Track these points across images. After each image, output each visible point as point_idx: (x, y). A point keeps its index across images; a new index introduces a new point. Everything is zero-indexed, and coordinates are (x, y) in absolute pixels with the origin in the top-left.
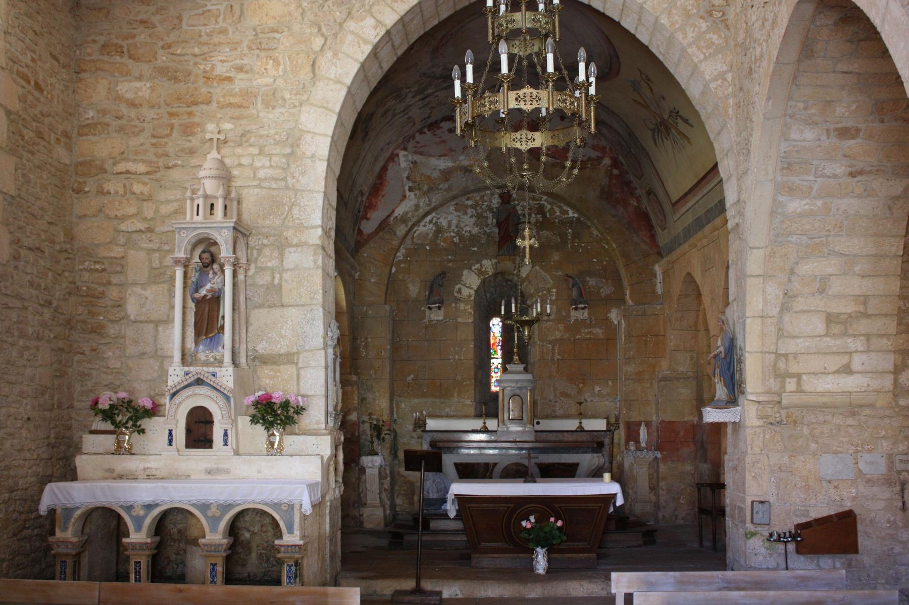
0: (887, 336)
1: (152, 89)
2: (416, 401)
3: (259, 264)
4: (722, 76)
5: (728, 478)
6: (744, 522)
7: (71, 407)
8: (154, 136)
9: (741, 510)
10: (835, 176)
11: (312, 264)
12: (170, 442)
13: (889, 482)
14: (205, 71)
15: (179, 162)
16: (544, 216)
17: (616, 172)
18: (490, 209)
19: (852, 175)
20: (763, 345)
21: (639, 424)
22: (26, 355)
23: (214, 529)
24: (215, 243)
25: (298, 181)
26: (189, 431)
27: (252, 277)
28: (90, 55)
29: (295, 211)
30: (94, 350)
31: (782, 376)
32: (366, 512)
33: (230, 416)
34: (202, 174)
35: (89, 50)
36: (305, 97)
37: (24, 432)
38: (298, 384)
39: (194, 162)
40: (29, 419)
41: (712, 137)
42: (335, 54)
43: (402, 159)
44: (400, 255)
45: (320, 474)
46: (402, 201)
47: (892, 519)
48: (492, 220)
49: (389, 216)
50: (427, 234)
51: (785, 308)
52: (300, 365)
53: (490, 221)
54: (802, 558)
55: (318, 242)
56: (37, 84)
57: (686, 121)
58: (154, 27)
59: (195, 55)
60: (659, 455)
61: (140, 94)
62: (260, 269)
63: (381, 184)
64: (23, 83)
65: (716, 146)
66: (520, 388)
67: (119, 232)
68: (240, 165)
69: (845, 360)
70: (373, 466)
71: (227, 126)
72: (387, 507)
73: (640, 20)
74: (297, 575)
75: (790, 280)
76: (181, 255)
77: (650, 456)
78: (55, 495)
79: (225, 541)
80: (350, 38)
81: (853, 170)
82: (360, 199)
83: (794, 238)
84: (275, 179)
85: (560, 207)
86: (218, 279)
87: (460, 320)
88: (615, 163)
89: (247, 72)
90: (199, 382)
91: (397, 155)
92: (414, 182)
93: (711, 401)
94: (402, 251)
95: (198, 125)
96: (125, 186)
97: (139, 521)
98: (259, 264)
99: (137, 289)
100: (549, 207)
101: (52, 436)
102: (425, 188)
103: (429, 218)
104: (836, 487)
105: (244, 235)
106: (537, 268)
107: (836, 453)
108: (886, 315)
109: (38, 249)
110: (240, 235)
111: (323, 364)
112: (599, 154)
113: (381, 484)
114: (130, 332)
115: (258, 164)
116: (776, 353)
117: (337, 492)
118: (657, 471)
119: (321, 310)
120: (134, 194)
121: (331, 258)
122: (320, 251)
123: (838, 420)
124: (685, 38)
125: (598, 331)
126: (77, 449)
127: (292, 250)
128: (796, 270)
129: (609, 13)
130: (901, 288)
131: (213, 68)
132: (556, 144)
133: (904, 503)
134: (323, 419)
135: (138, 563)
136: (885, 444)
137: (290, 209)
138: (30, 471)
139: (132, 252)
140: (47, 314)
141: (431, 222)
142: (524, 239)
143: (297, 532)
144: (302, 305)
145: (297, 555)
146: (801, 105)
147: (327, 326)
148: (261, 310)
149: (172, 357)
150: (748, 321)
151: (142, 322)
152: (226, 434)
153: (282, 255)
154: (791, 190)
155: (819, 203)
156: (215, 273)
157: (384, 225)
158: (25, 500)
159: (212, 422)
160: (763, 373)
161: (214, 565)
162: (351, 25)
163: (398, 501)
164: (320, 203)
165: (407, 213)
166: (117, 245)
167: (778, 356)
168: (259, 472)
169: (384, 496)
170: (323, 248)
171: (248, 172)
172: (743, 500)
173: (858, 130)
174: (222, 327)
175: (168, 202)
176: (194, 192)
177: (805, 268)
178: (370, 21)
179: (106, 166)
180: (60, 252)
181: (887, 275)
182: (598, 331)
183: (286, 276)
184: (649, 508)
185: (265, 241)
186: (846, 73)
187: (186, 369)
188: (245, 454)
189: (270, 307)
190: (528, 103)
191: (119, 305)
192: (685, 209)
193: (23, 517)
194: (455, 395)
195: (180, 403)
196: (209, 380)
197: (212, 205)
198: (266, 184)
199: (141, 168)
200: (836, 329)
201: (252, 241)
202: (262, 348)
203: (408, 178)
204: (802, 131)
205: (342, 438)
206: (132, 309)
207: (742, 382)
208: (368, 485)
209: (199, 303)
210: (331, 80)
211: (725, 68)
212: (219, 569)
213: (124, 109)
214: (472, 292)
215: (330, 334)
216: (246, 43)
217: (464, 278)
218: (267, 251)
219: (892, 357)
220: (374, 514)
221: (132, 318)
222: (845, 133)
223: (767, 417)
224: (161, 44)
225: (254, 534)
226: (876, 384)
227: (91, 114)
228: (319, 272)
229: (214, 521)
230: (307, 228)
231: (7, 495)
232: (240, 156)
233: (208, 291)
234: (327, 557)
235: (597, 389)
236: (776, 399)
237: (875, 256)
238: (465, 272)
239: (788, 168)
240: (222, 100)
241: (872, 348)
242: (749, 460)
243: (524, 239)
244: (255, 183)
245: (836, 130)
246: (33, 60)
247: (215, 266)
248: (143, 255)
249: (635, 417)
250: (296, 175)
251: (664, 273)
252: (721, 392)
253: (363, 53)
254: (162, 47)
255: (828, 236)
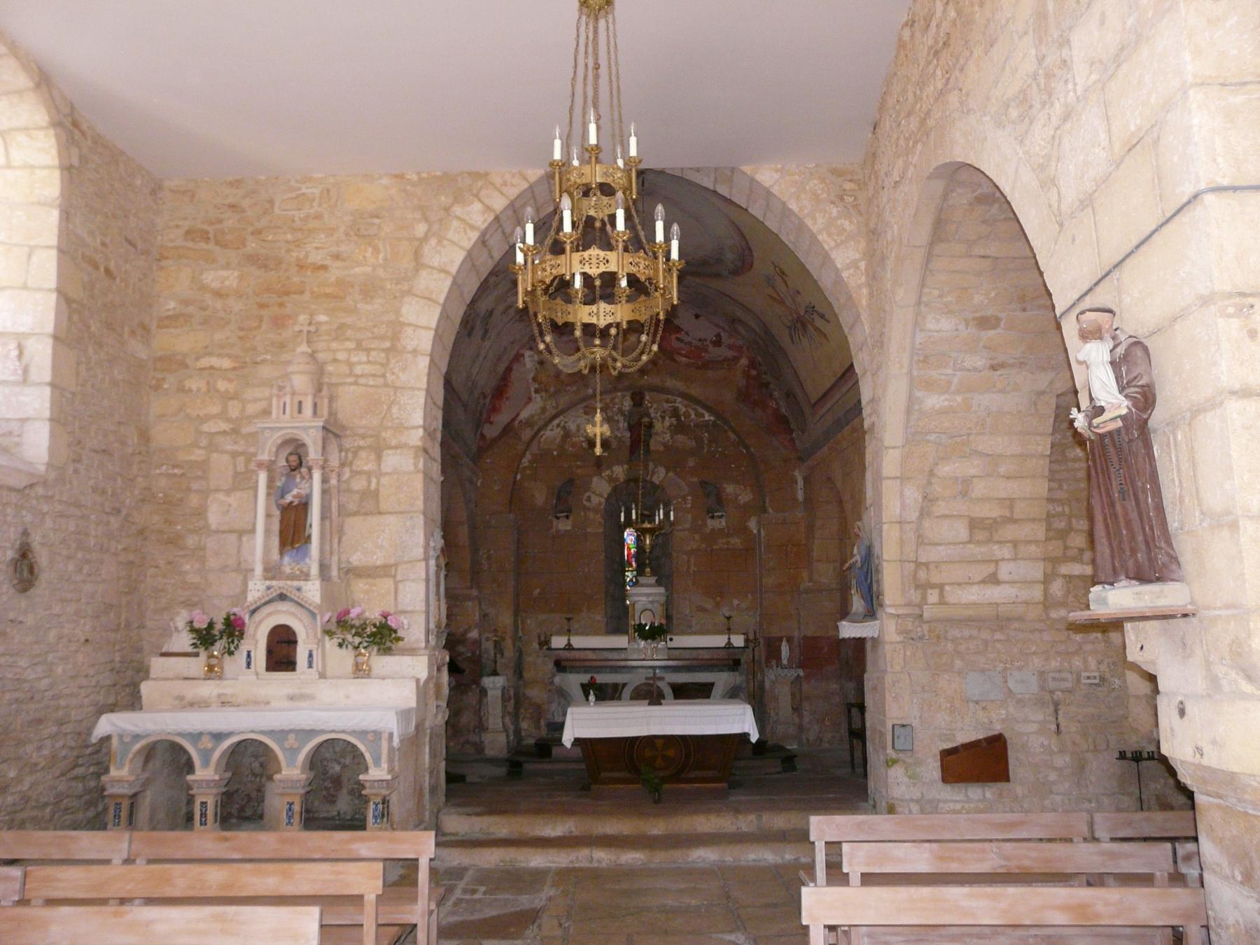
0: (1036, 542)
1: (241, 278)
2: (542, 617)
3: (354, 468)
4: (854, 264)
5: (869, 702)
6: (884, 748)
7: (142, 626)
8: (241, 329)
9: (882, 735)
10: (975, 369)
11: (412, 468)
12: (249, 665)
13: (1040, 702)
14: (298, 259)
15: (269, 357)
16: (679, 419)
17: (754, 373)
18: (621, 411)
19: (993, 368)
20: (902, 553)
21: (780, 640)
22: (86, 569)
23: (291, 763)
24: (304, 445)
25: (398, 377)
26: (270, 652)
27: (347, 482)
28: (172, 241)
29: (395, 410)
30: (169, 563)
31: (923, 587)
32: (487, 738)
33: (315, 635)
34: (291, 369)
35: (172, 236)
36: (406, 287)
37: (80, 657)
38: (396, 599)
39: (286, 357)
40: (87, 640)
41: (846, 330)
42: (439, 242)
43: (527, 360)
44: (525, 461)
45: (415, 698)
46: (527, 403)
47: (1046, 743)
48: (623, 425)
49: (513, 420)
50: (555, 439)
51: (924, 513)
52: (399, 578)
53: (621, 425)
54: (948, 787)
55: (419, 443)
56: (107, 271)
57: (822, 316)
58: (243, 211)
59: (287, 242)
60: (802, 674)
61: (227, 283)
62: (355, 473)
63: (506, 385)
64: (90, 269)
65: (850, 339)
66: (652, 602)
67: (201, 433)
68: (335, 360)
69: (990, 569)
70: (494, 688)
71: (322, 318)
72: (511, 732)
73: (768, 205)
74: (384, 814)
75: (929, 483)
76: (265, 457)
77: (793, 673)
78: (106, 725)
79: (304, 776)
80: (455, 223)
81: (995, 362)
82: (482, 401)
83: (932, 437)
84: (374, 375)
85: (695, 410)
86: (304, 485)
87: (589, 530)
88: (753, 364)
89: (344, 260)
90: (282, 597)
91: (523, 355)
92: (540, 383)
93: (844, 613)
94: (528, 456)
95: (289, 317)
96: (208, 383)
97: (206, 755)
98: (354, 468)
99: (221, 496)
100: (684, 410)
101: (117, 659)
102: (552, 390)
103: (557, 421)
104: (984, 708)
105: (337, 436)
106: (671, 474)
107: (983, 671)
108: (1034, 520)
109: (104, 451)
110: (331, 436)
111: (423, 576)
112: (735, 354)
113: (504, 707)
114: (211, 543)
115: (354, 359)
116: (916, 562)
117: (440, 717)
118: (800, 690)
119: (422, 517)
120: (218, 391)
121: (434, 460)
122: (421, 453)
123: (985, 635)
124: (815, 223)
125: (736, 542)
126: (143, 672)
127: (390, 452)
128: (935, 471)
129: (735, 199)
130: (1050, 490)
131: (306, 256)
132: (638, 318)
133: (1058, 726)
134: (423, 637)
135: (204, 804)
136: (1036, 661)
137: (390, 408)
138: (86, 700)
139: (215, 455)
140: (115, 522)
141: (558, 425)
142: (594, 425)
143: (385, 766)
144: (402, 513)
145: (384, 792)
146: (936, 293)
147: (428, 536)
148: (356, 518)
149: (253, 570)
150: (885, 527)
151: (224, 532)
152: (311, 656)
153: (379, 458)
154: (929, 385)
155: (959, 399)
156: (303, 478)
157: (508, 430)
158: (79, 734)
159: (296, 642)
160: (903, 583)
161: (291, 804)
162: (457, 210)
163: (524, 725)
164: (422, 401)
165: (533, 416)
166: (200, 447)
167: (918, 565)
168: (347, 697)
169: (507, 720)
170: (426, 451)
171: (344, 369)
172: (883, 723)
173: (998, 320)
174: (309, 537)
175: (256, 400)
176: (281, 388)
177: (945, 469)
178: (477, 206)
179: (188, 361)
180: (133, 455)
181: (1033, 476)
182: (736, 542)
183: (384, 480)
184: (792, 730)
185: (362, 443)
186: (983, 257)
187: (268, 583)
188: (333, 678)
189: (366, 514)
190: (594, 266)
191: (201, 513)
192: (824, 410)
193: (75, 753)
194: (585, 609)
195: (261, 622)
196: (294, 595)
197: (300, 403)
198: (362, 381)
199: (226, 363)
200: (980, 535)
201: (347, 443)
202: (356, 559)
203: (534, 379)
204: (938, 321)
205: (448, 659)
206: (214, 518)
207: (880, 594)
208: (490, 710)
209: (286, 509)
210: (433, 268)
211: (857, 256)
212: (297, 808)
213: (209, 300)
214: (603, 500)
215: (432, 544)
216: (342, 229)
217: (593, 485)
218: (363, 454)
219: (1041, 565)
220: (496, 741)
221: (213, 527)
222: (984, 323)
223: (907, 632)
224: (250, 229)
225: (344, 766)
226: (1025, 594)
227: (172, 305)
228: (420, 476)
229: (294, 751)
230: (407, 428)
231: (55, 729)
232: (334, 351)
233: (294, 497)
234: (427, 791)
235: (736, 602)
236: (917, 611)
237: (1021, 455)
238: (595, 479)
239: (924, 361)
240: (315, 289)
241: (1020, 555)
242: (888, 679)
243: (594, 425)
244: (351, 380)
245: (975, 319)
246: (103, 244)
247: (304, 470)
248: (226, 458)
249: (775, 632)
250: (396, 370)
251: (806, 479)
252: (858, 604)
253: (469, 239)
254: (252, 233)
255: (969, 434)
